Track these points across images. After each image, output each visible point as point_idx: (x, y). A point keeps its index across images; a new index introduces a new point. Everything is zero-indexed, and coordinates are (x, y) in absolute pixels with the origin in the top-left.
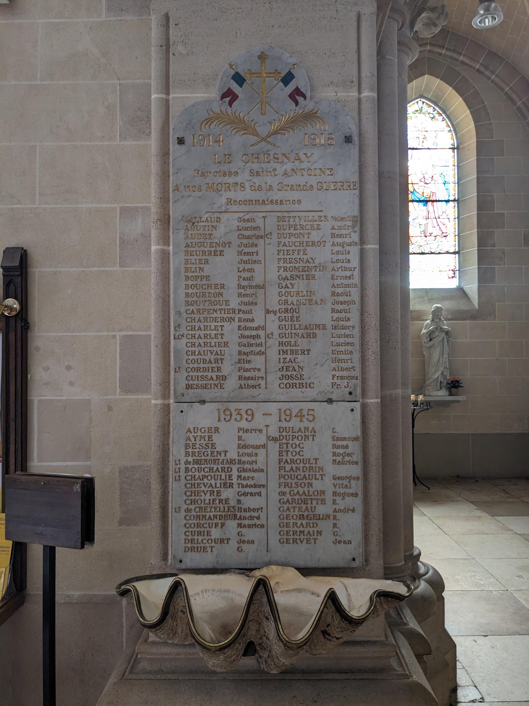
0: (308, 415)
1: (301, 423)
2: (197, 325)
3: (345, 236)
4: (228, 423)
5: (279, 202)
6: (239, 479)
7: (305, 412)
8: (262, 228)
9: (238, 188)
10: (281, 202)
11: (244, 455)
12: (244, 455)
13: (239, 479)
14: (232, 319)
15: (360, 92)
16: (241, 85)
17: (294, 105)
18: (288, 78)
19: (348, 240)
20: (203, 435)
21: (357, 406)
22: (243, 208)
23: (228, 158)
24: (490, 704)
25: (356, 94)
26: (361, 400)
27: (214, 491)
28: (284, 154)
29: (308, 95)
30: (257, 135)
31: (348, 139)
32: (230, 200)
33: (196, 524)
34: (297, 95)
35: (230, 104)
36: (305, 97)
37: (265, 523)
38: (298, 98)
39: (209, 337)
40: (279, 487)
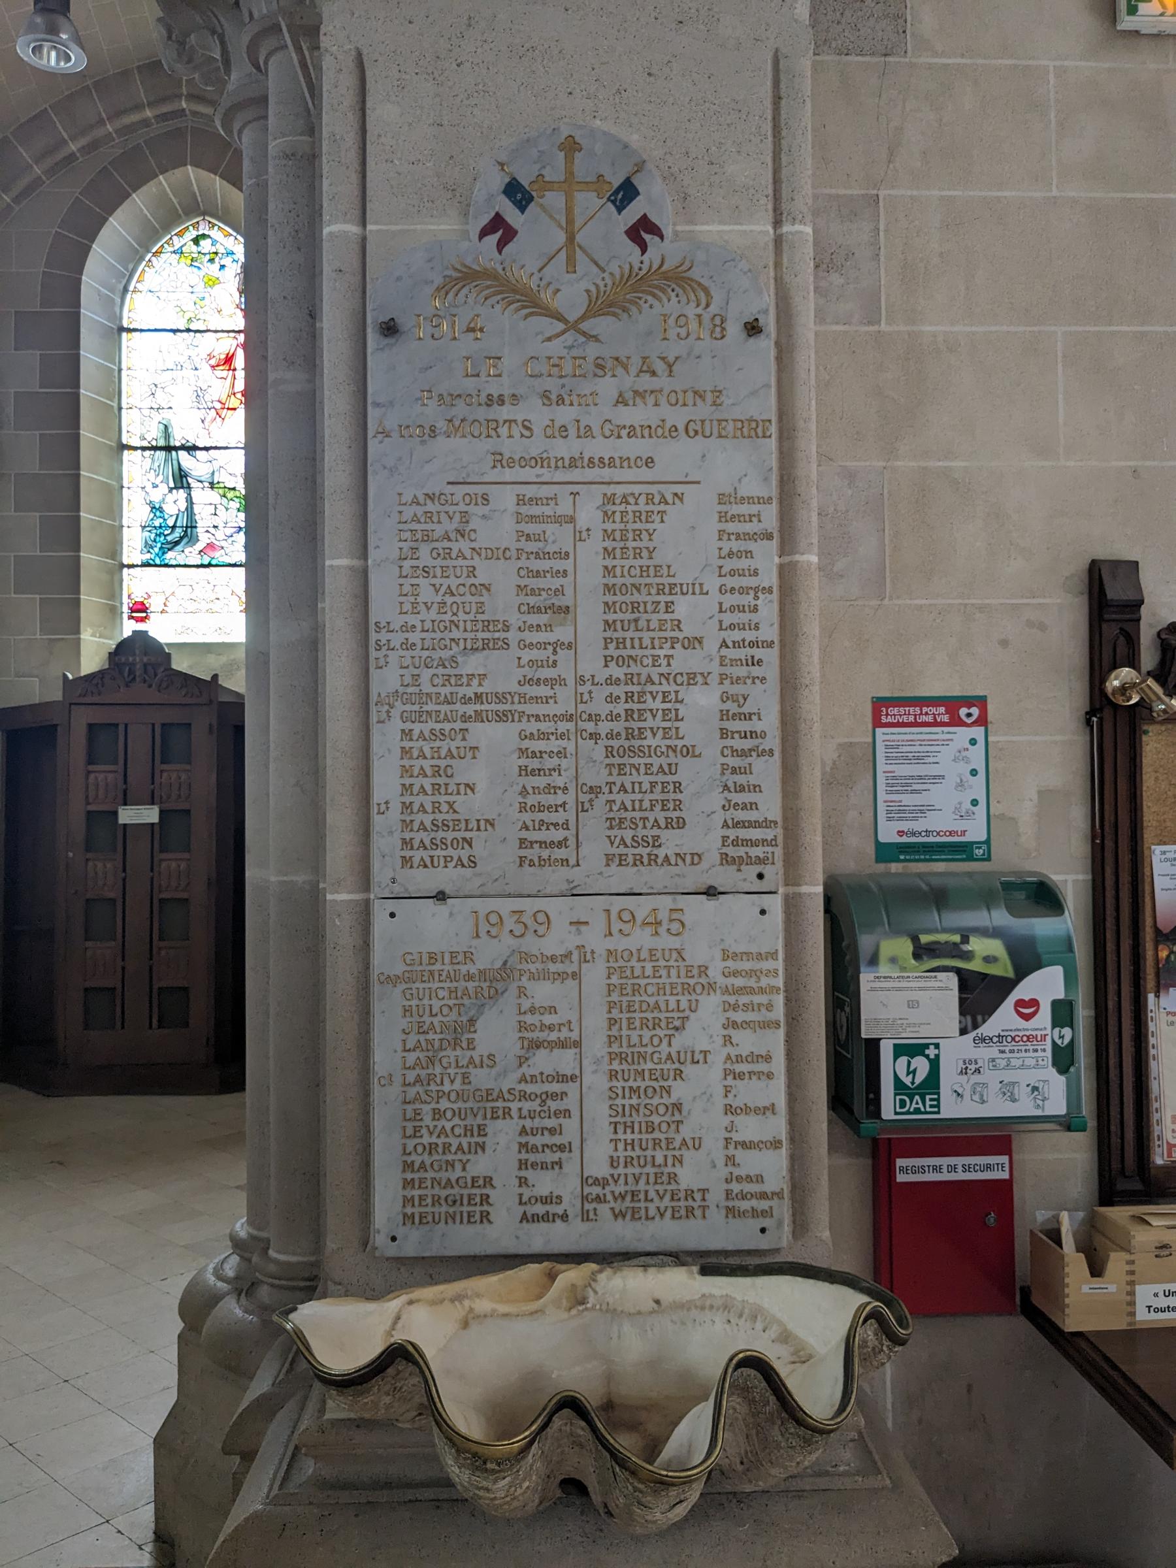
1: (656, 938)
3: (747, 518)
4: (496, 940)
6: (523, 1151)
10: (611, 463)
11: (533, 1201)
12: (533, 1201)
13: (523, 1151)
16: (522, 209)
17: (638, 250)
18: (626, 193)
20: (451, 1210)
21: (775, 904)
24: (1167, 978)
28: (617, 359)
33: (428, 1147)
34: (643, 231)
38: (647, 237)
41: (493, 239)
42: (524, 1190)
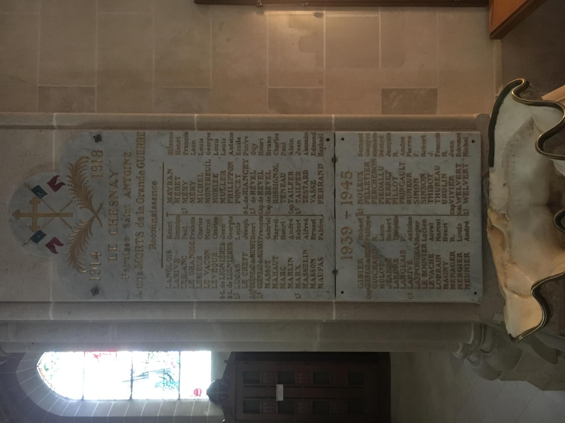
0: (346, 177)
2: (295, 282)
5: (154, 201)
7: (344, 180)
8: (389, 217)
9: (140, 239)
14: (424, 246)
15: (52, 128)
17: (63, 187)
18: (38, 191)
19: (183, 141)
21: (339, 134)
22: (159, 234)
23: (112, 247)
25: (54, 131)
26: (333, 132)
27: (362, 268)
29: (55, 174)
30: (92, 220)
31: (98, 139)
32: (151, 246)
35: (60, 244)
36: (57, 176)
37: (213, 217)
38: (58, 182)
39: (291, 271)
40: (240, 202)
41: (57, 248)
42: (456, 239)
